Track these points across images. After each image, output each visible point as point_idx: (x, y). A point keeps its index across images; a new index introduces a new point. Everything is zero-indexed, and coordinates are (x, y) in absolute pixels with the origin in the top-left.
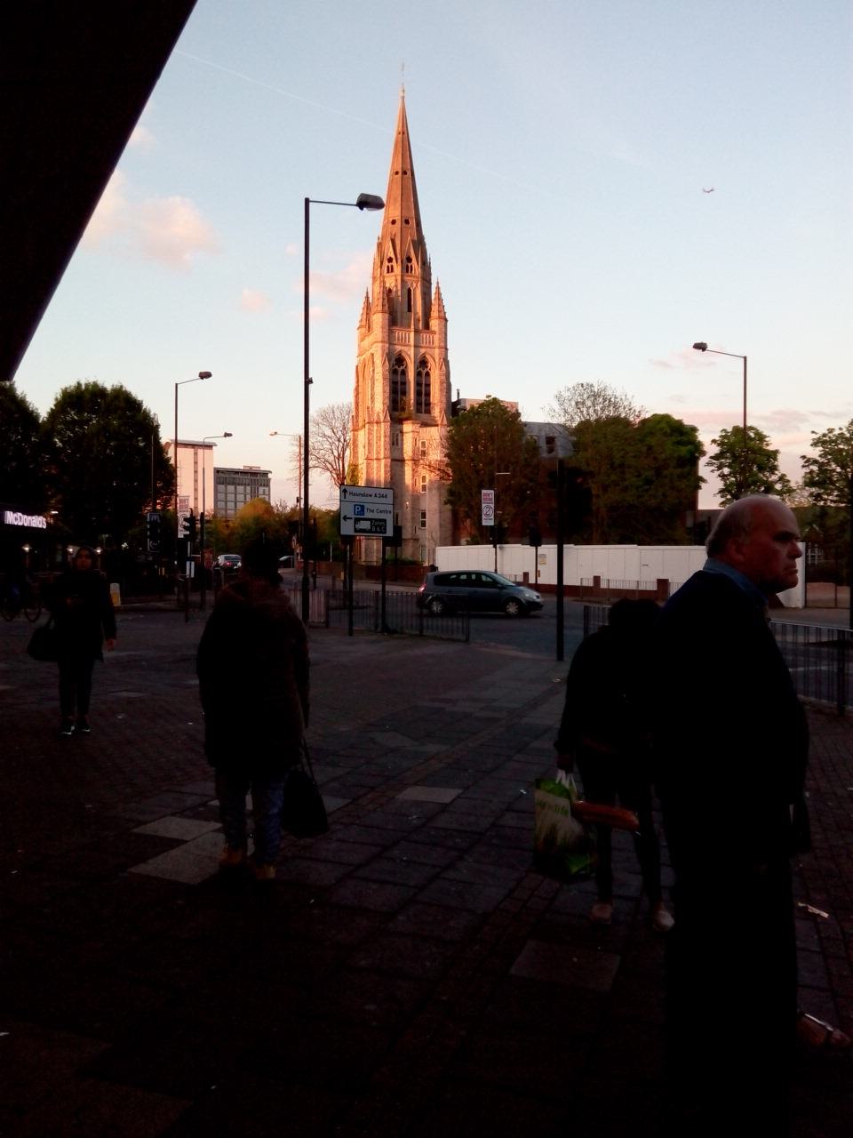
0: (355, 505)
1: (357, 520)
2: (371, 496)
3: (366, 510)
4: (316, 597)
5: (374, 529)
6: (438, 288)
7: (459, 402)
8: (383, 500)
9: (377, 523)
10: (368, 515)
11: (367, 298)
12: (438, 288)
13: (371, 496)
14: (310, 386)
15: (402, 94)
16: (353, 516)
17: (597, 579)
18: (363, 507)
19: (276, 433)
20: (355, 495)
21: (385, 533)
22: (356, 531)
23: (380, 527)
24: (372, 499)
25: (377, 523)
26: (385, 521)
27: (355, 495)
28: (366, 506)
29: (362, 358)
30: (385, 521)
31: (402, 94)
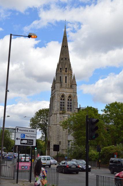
0: (21, 134)
1: (22, 140)
2: (28, 131)
3: (25, 136)
4: (4, 168)
5: (28, 143)
6: (74, 76)
7: (80, 108)
8: (32, 133)
9: (29, 141)
10: (26, 138)
11: (54, 79)
12: (74, 76)
13: (28, 131)
14: (8, 93)
15: (65, 27)
16: (20, 138)
17: (99, 168)
18: (24, 135)
19: (26, 117)
20: (21, 130)
21: (33, 145)
22: (21, 144)
23: (31, 142)
24: (28, 132)
25: (29, 141)
26: (33, 140)
27: (21, 130)
28: (26, 135)
29: (52, 96)
30: (33, 140)
31: (65, 27)
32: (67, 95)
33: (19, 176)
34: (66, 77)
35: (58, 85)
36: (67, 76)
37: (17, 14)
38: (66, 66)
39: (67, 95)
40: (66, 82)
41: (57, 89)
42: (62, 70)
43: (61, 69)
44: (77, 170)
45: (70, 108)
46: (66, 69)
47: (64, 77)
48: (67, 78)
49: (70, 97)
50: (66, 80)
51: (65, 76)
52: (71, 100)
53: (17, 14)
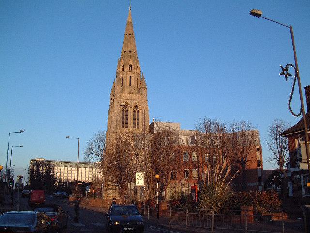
12: (143, 76)
32: (132, 104)
33: (295, 45)
34: (131, 78)
35: (118, 88)
36: (132, 76)
37: (57, 183)
38: (131, 62)
39: (132, 104)
40: (130, 85)
41: (117, 95)
42: (124, 67)
43: (123, 66)
44: (12, 227)
45: (136, 123)
46: (131, 66)
47: (128, 78)
48: (128, 85)
49: (136, 107)
50: (130, 82)
51: (130, 75)
52: (138, 111)
53: (57, 183)
